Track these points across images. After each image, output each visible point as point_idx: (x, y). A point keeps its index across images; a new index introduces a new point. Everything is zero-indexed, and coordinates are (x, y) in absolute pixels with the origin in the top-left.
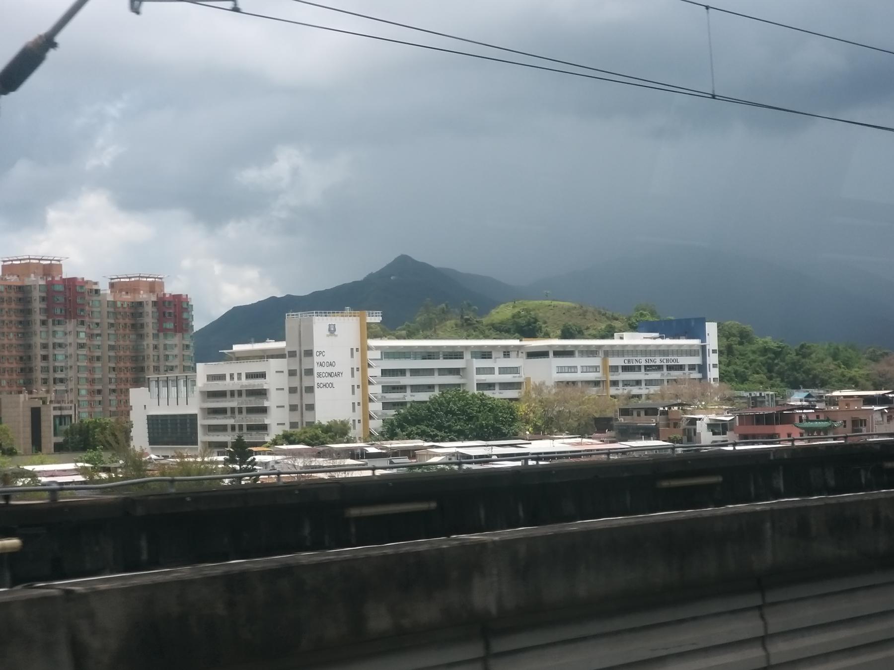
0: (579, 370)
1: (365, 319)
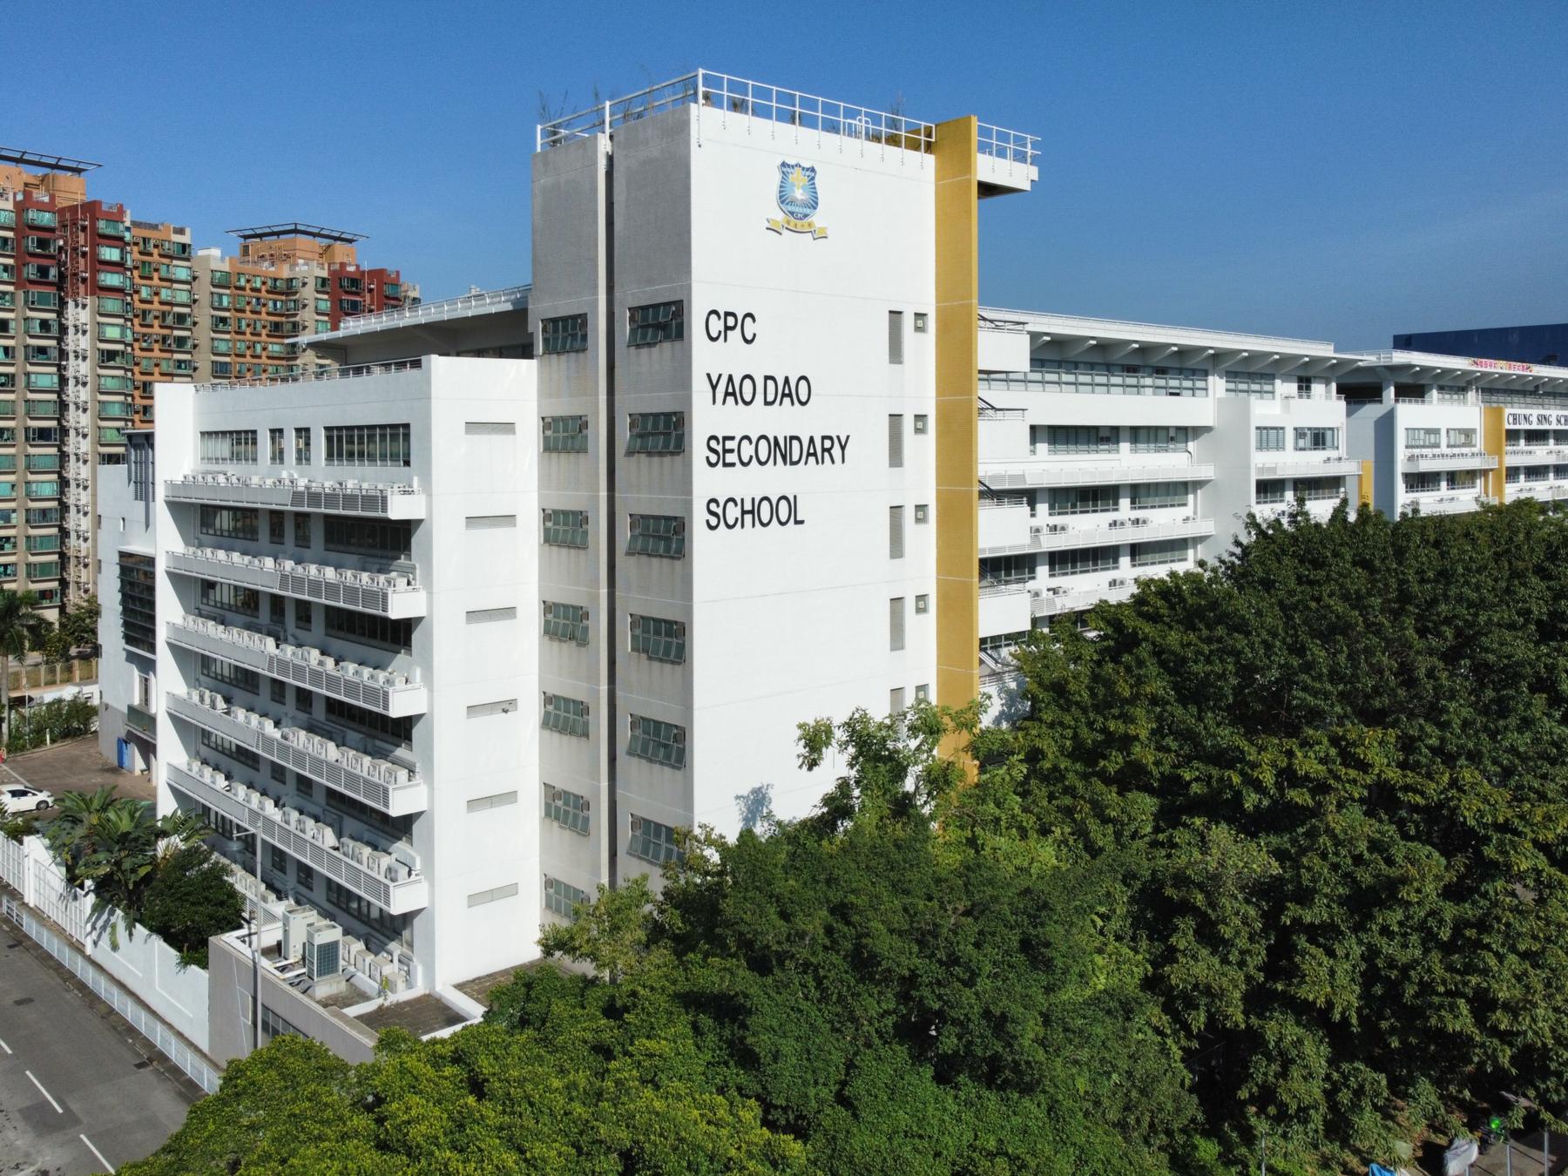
1: (966, 165)
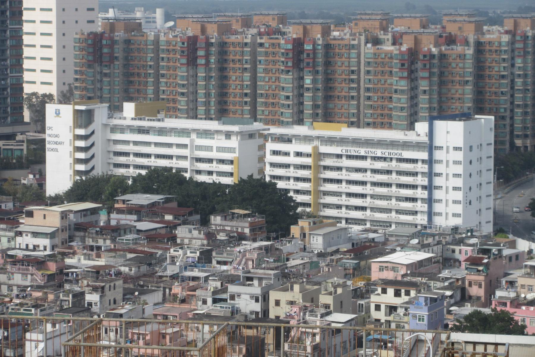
0: (292, 154)
